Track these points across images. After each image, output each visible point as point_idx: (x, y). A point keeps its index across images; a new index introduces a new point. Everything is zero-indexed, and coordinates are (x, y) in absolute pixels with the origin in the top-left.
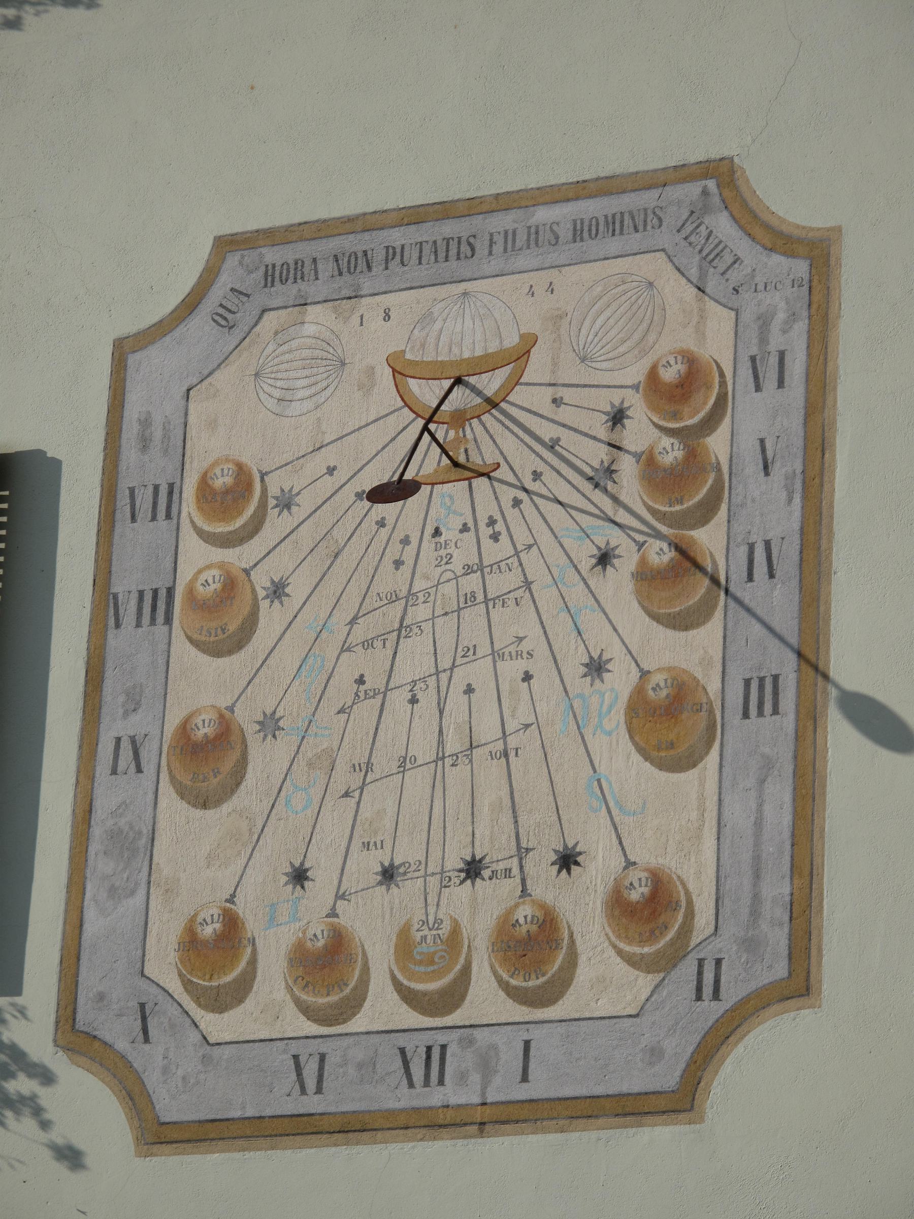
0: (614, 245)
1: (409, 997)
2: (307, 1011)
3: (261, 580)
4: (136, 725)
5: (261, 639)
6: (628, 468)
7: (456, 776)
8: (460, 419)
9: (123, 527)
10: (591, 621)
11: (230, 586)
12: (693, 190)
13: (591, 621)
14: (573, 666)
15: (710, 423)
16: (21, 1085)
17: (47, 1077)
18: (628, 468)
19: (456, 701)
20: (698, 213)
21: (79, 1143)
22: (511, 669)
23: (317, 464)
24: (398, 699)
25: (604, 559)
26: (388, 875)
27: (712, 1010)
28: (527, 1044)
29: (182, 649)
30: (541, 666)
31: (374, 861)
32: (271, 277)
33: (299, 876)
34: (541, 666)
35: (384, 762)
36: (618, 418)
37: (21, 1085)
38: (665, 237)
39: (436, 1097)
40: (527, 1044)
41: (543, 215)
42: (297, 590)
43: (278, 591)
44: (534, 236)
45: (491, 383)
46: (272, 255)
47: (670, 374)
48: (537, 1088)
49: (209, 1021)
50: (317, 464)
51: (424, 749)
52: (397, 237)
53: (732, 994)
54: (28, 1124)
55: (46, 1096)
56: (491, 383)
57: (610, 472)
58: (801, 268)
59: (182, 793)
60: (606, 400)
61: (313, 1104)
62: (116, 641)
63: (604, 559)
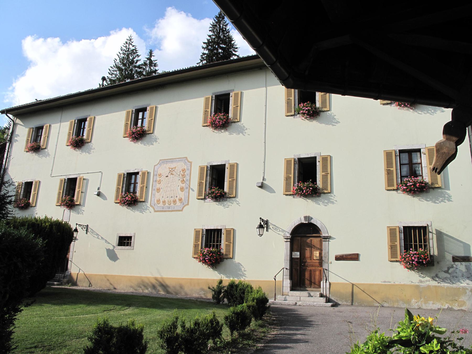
0: (180, 162)
1: (168, 204)
2: (163, 205)
3: (161, 180)
4: (154, 188)
5: (161, 183)
6: (181, 174)
7: (171, 192)
8: (172, 171)
9: (154, 177)
10: (179, 184)
11: (160, 180)
12: (185, 159)
13: (179, 184)
14: (177, 186)
15: (185, 172)
16: (148, 208)
17: (149, 208)
18: (181, 174)
19: (171, 188)
20: (185, 160)
21: (337, 200)
22: (174, 186)
23: (164, 174)
24: (168, 187)
25: (179, 180)
26: (167, 197)
27: (183, 205)
28: (338, 258)
29: (157, 184)
30: (176, 186)
31: (167, 196)
32: (162, 162)
33: (163, 197)
34: (176, 186)
35: (167, 191)
36: (180, 172)
37: (148, 208)
38: (183, 161)
39: (170, 210)
40: (338, 258)
41: (177, 160)
42: (163, 181)
43: (162, 181)
44: (176, 161)
45: (174, 169)
46: (163, 161)
47: (183, 169)
48: (175, 209)
49: (158, 205)
50: (164, 174)
51: (169, 190)
52: (169, 160)
53: (184, 205)
54: (148, 210)
55: (149, 209)
56: (174, 169)
57: (180, 175)
58: (190, 164)
59: (157, 192)
60: (180, 171)
61: (163, 210)
62: (154, 183)
63: (179, 180)
